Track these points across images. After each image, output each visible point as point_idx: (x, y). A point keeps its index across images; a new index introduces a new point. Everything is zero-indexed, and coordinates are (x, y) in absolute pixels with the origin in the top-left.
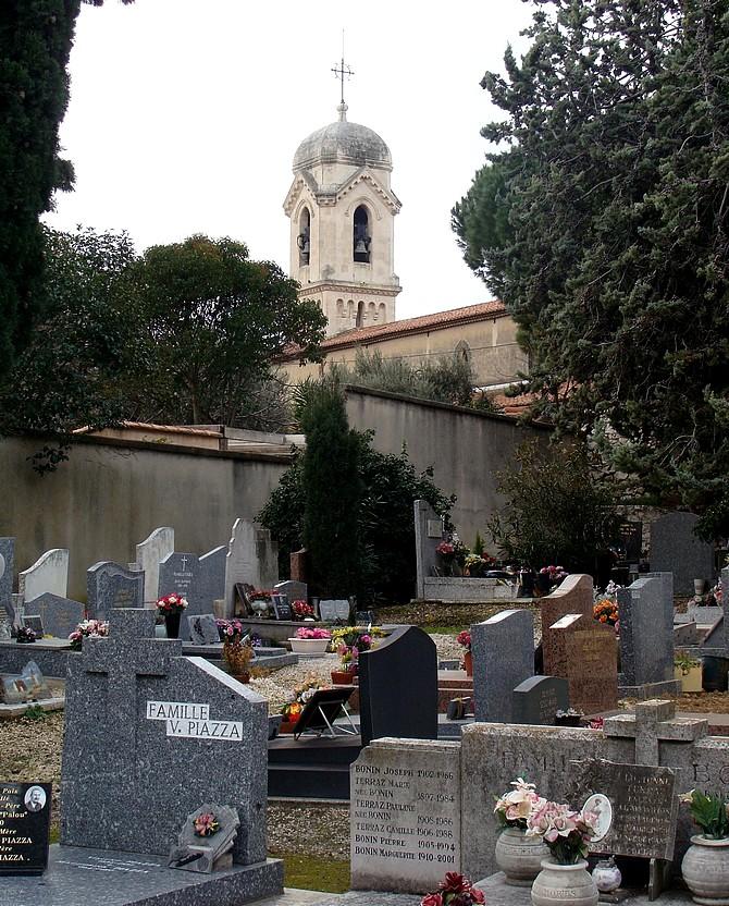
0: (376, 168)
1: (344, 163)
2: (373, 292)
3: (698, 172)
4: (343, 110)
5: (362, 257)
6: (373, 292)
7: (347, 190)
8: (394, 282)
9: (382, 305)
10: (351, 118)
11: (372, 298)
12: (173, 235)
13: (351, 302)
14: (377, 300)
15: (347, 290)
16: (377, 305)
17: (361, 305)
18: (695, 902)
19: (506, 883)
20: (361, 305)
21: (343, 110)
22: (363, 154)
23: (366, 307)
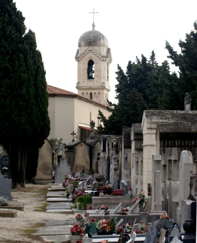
0: (96, 46)
1: (84, 46)
2: (95, 89)
3: (12, 25)
4: (94, 26)
5: (90, 78)
6: (95, 89)
7: (83, 55)
8: (103, 85)
9: (99, 93)
10: (96, 29)
11: (95, 91)
12: (122, 69)
13: (87, 93)
14: (97, 92)
15: (85, 89)
16: (97, 93)
17: (91, 94)
18: (156, 238)
19: (192, 171)
20: (91, 94)
21: (94, 26)
22: (91, 42)
23: (93, 95)
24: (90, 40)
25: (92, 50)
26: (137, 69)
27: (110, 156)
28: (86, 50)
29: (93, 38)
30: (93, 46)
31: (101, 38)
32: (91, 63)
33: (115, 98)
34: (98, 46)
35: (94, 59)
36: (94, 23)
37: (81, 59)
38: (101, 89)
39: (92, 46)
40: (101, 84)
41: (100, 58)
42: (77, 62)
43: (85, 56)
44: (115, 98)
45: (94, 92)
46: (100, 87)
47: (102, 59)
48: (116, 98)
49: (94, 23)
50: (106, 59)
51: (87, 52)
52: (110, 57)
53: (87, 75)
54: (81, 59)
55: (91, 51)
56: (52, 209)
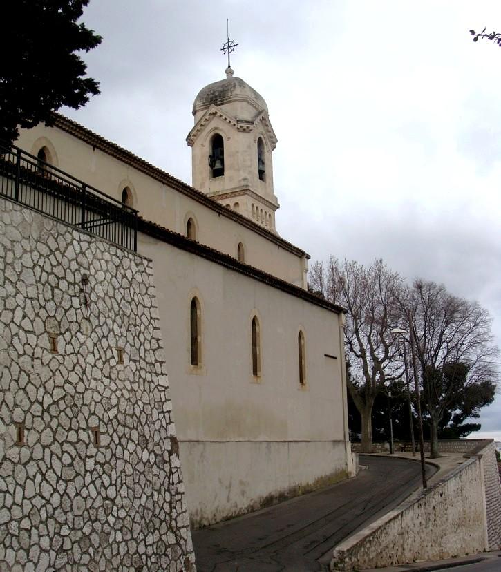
0: (226, 103)
22: (216, 97)
24: (213, 94)
25: (216, 113)
26: (391, 291)
27: (352, 300)
28: (204, 115)
29: (221, 89)
30: (220, 105)
31: (237, 84)
32: (217, 142)
33: (96, 92)
34: (230, 102)
35: (222, 130)
36: (229, 67)
37: (194, 136)
38: (240, 195)
39: (217, 105)
40: (240, 181)
41: (234, 125)
42: (190, 148)
43: (203, 128)
44: (96, 92)
45: (234, 203)
46: (235, 188)
47: (239, 125)
48: (92, 87)
49: (229, 67)
50: (248, 128)
51: (207, 117)
52: (270, 132)
53: (209, 168)
54: (194, 136)
55: (214, 114)
56: (255, 344)
